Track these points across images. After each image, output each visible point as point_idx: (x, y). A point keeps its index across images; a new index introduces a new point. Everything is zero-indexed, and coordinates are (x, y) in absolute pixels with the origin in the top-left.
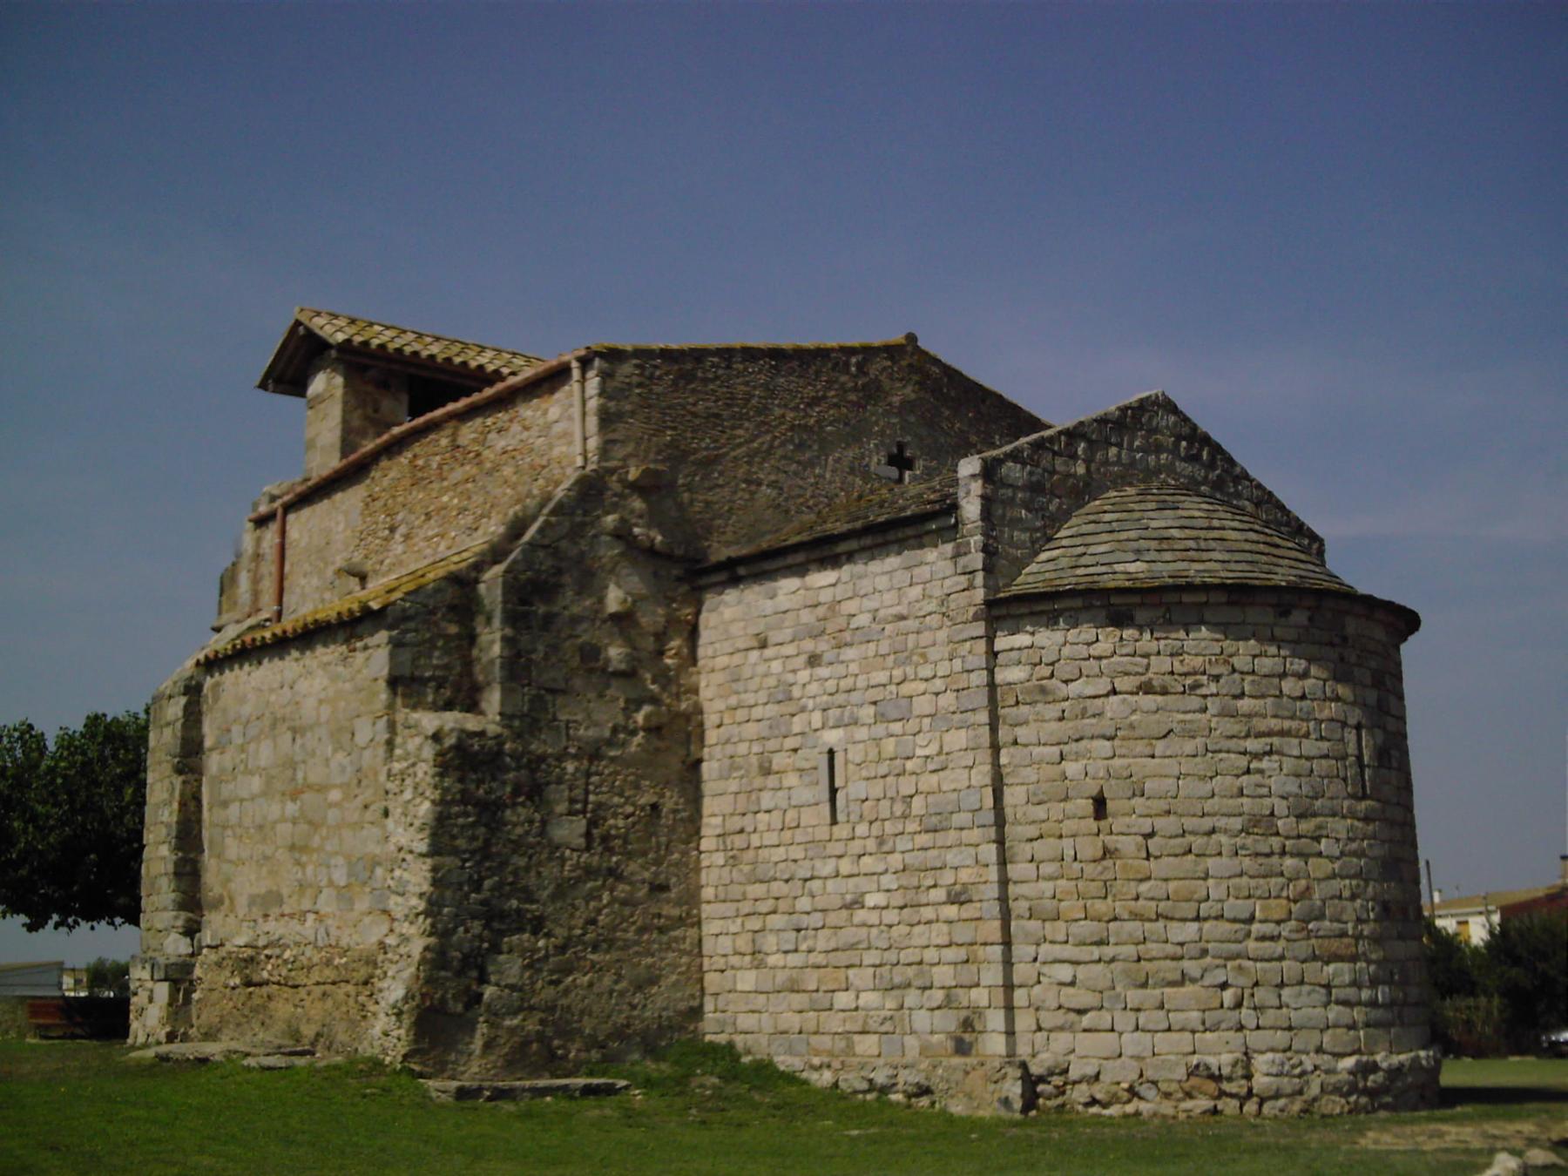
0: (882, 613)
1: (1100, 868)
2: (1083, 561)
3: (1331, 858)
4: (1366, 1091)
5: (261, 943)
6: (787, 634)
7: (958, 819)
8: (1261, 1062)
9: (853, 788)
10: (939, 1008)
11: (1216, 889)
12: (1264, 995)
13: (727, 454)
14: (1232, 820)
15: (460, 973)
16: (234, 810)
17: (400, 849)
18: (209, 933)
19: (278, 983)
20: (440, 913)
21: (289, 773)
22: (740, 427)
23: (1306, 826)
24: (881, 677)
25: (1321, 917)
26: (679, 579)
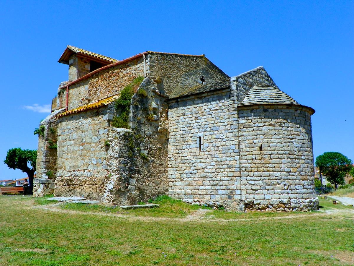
0: (212, 109)
1: (261, 161)
2: (255, 99)
3: (304, 160)
4: (311, 206)
5: (72, 176)
6: (190, 113)
7: (229, 151)
8: (292, 200)
9: (205, 144)
10: (225, 189)
11: (284, 166)
12: (292, 187)
13: (173, 76)
14: (287, 152)
15: (124, 182)
16: (66, 148)
17: (111, 156)
18: (58, 174)
19: (77, 185)
20: (120, 170)
21: (81, 140)
22: (175, 70)
23: (300, 153)
24: (213, 122)
25: (302, 171)
26: (165, 101)
